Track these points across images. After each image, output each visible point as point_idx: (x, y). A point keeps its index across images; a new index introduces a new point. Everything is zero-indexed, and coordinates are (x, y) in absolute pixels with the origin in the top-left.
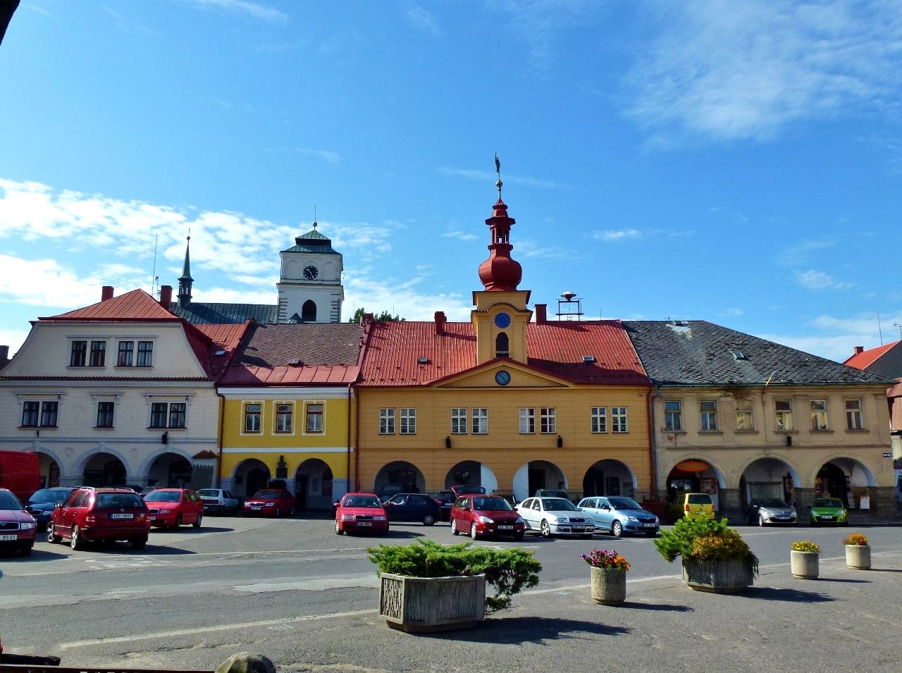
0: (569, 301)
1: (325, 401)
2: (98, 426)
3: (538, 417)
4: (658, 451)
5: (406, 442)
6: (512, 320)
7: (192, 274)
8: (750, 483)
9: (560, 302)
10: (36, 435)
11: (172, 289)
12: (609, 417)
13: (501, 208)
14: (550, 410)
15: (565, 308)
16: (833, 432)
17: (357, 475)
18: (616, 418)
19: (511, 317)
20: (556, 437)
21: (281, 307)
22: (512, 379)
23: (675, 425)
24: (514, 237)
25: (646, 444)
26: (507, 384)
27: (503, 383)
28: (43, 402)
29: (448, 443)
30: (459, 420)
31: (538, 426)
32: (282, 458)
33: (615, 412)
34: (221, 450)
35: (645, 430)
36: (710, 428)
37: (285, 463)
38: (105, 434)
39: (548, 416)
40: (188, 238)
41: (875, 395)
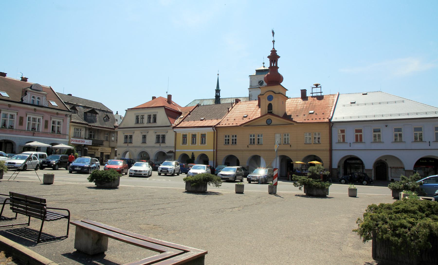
0: (317, 87)
1: (206, 133)
2: (142, 143)
5: (234, 147)
6: (274, 97)
7: (220, 89)
8: (390, 167)
9: (313, 88)
10: (159, 146)
11: (171, 95)
12: (231, 138)
13: (274, 52)
15: (315, 90)
17: (216, 160)
18: (226, 139)
19: (273, 96)
20: (290, 145)
21: (250, 98)
22: (272, 121)
24: (279, 61)
25: (328, 148)
27: (269, 123)
28: (129, 135)
32: (193, 153)
34: (175, 150)
37: (194, 155)
38: (144, 145)
39: (286, 137)
40: (218, 74)
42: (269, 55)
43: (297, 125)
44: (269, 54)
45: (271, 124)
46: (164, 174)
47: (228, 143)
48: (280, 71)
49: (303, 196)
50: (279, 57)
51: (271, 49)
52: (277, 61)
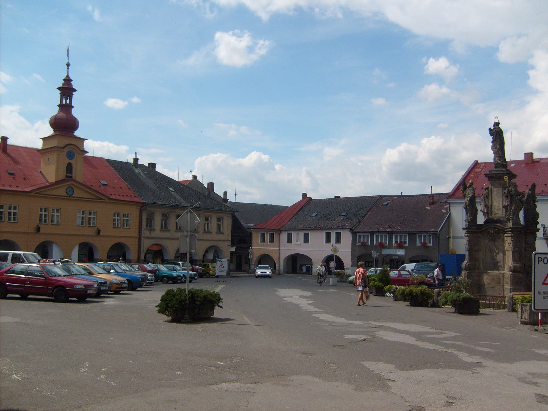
3: (86, 216)
4: (142, 239)
7: (67, 67)
13: (68, 80)
14: (118, 214)
16: (211, 233)
20: (95, 229)
23: (150, 226)
26: (71, 195)
29: (38, 229)
30: (92, 218)
31: (86, 221)
33: (10, 208)
35: (138, 227)
36: (165, 226)
39: (12, 211)
41: (228, 216)
42: (61, 85)
43: (109, 201)
44: (60, 84)
45: (74, 195)
46: (402, 276)
47: (45, 221)
48: (75, 112)
49: (409, 306)
50: (75, 90)
51: (64, 77)
52: (72, 97)
